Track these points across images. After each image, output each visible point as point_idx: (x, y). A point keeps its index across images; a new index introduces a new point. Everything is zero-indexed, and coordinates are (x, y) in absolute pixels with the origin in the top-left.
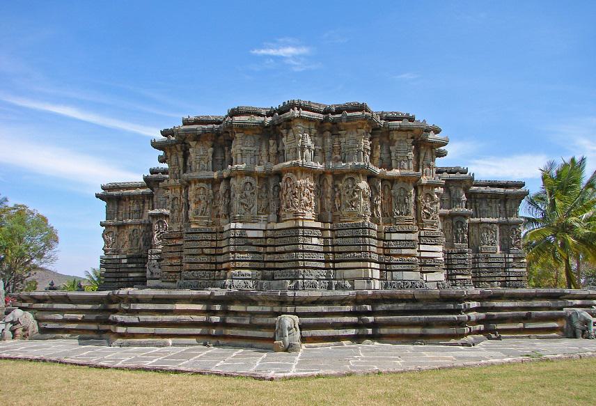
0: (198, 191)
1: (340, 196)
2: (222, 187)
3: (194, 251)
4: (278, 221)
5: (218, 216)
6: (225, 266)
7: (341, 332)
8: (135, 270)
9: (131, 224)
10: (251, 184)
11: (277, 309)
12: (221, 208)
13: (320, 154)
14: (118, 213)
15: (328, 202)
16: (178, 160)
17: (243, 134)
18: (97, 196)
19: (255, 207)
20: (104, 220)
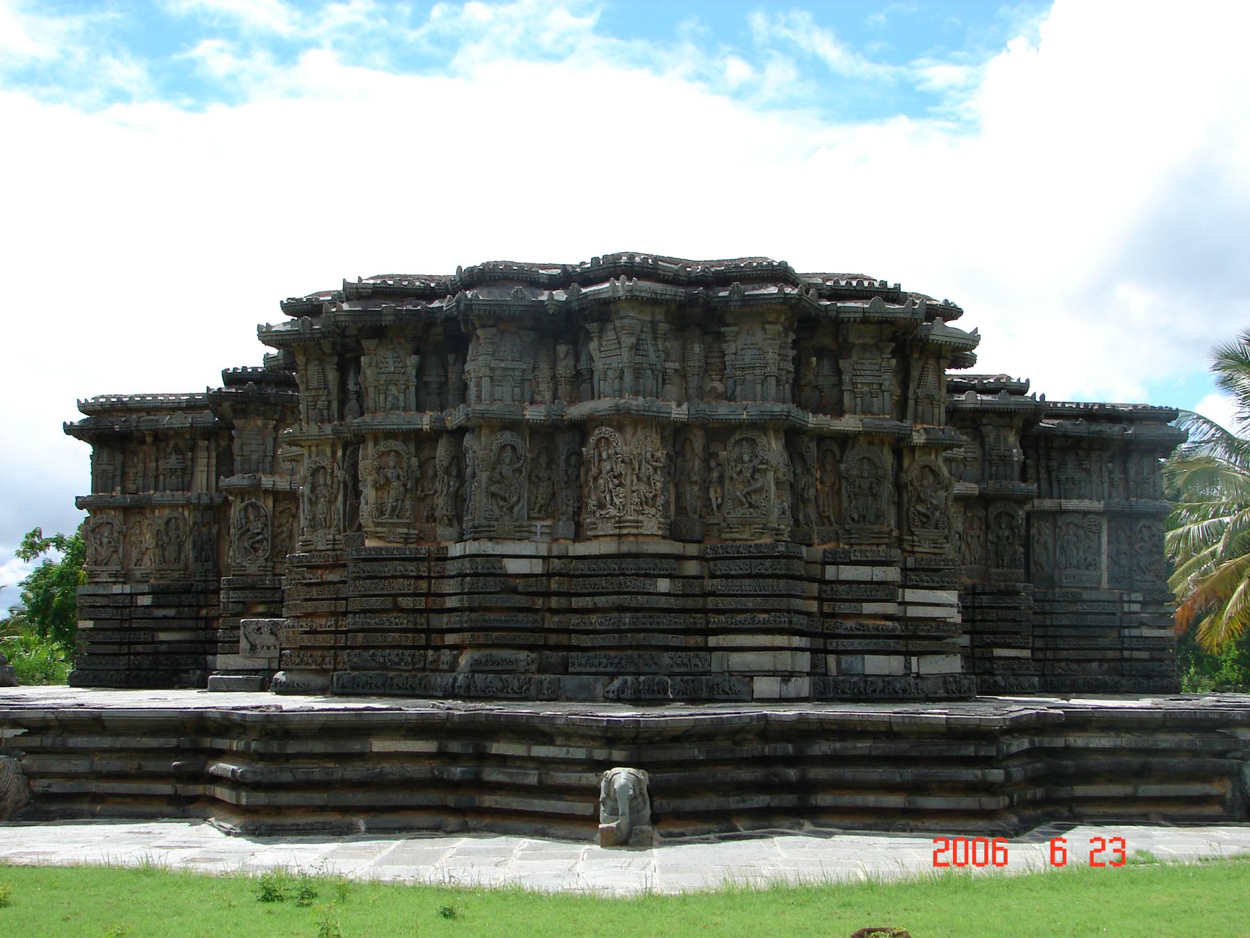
0: (384, 458)
1: (721, 477)
2: (442, 451)
3: (375, 603)
4: (578, 537)
5: (431, 518)
6: (450, 639)
7: (733, 803)
8: (175, 623)
9: (162, 506)
10: (513, 448)
11: (600, 754)
12: (440, 501)
13: (676, 379)
14: (124, 475)
15: (692, 492)
16: (325, 377)
17: (494, 330)
18: (70, 429)
19: (524, 502)
20: (86, 490)
